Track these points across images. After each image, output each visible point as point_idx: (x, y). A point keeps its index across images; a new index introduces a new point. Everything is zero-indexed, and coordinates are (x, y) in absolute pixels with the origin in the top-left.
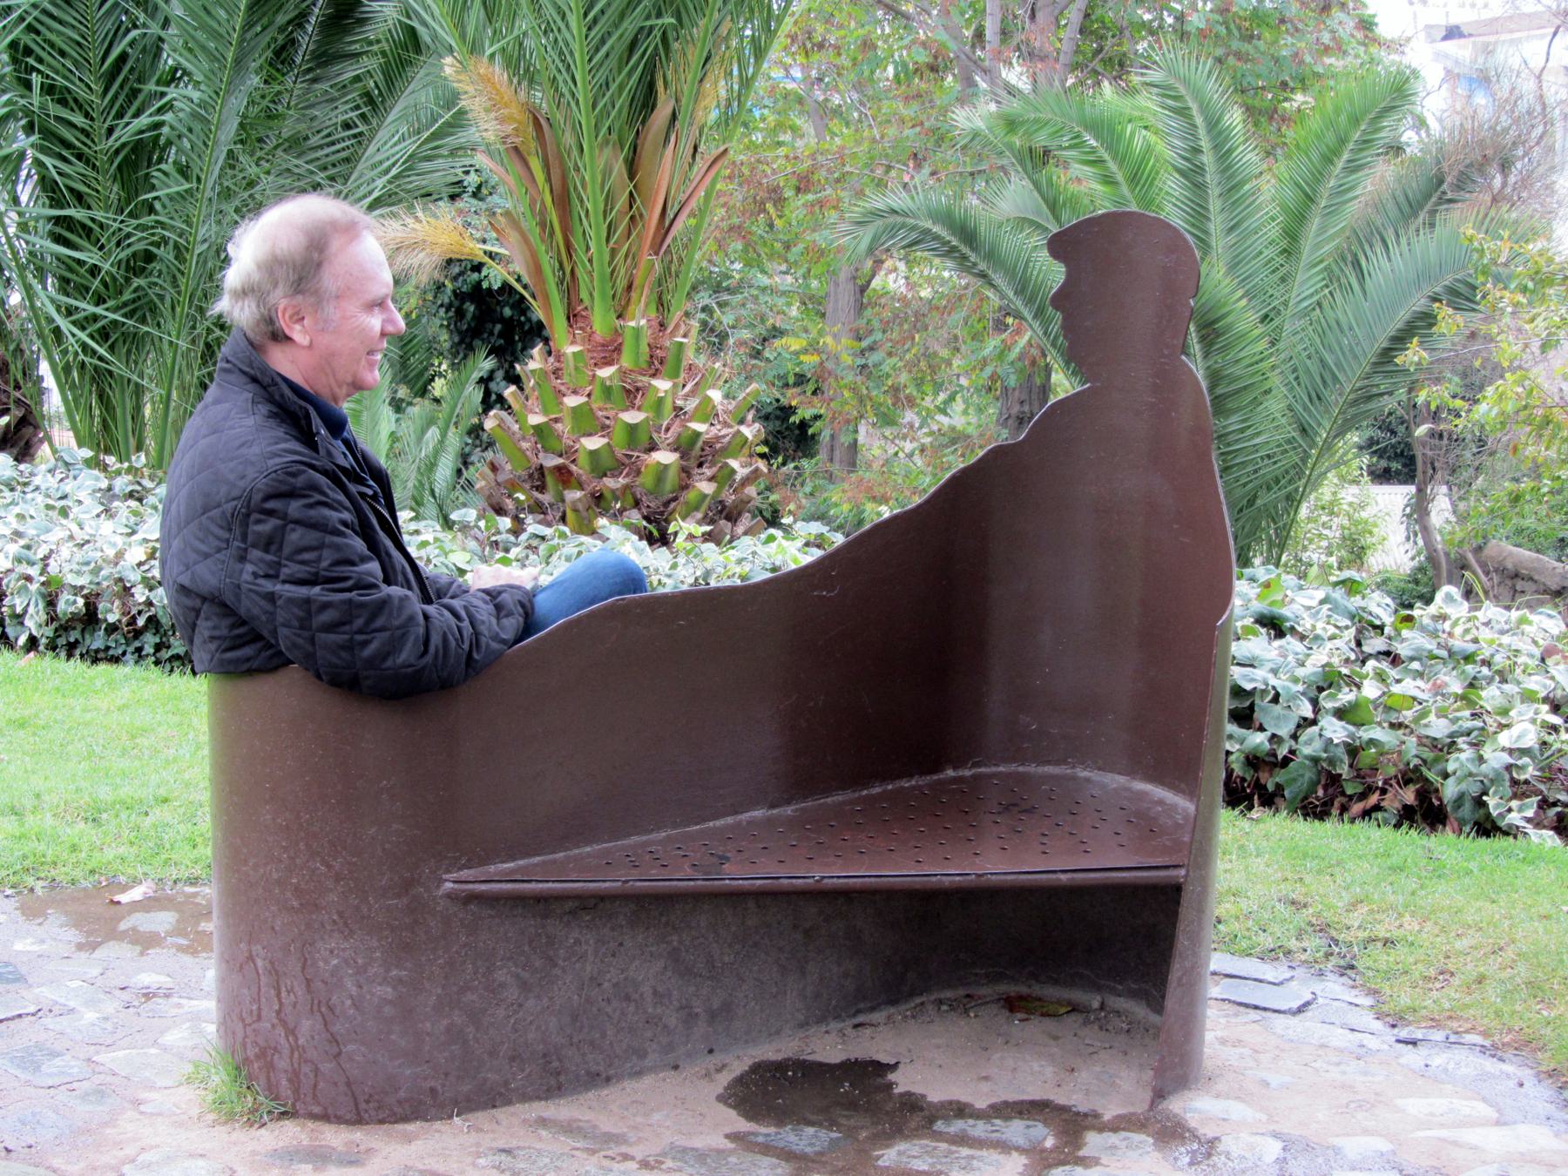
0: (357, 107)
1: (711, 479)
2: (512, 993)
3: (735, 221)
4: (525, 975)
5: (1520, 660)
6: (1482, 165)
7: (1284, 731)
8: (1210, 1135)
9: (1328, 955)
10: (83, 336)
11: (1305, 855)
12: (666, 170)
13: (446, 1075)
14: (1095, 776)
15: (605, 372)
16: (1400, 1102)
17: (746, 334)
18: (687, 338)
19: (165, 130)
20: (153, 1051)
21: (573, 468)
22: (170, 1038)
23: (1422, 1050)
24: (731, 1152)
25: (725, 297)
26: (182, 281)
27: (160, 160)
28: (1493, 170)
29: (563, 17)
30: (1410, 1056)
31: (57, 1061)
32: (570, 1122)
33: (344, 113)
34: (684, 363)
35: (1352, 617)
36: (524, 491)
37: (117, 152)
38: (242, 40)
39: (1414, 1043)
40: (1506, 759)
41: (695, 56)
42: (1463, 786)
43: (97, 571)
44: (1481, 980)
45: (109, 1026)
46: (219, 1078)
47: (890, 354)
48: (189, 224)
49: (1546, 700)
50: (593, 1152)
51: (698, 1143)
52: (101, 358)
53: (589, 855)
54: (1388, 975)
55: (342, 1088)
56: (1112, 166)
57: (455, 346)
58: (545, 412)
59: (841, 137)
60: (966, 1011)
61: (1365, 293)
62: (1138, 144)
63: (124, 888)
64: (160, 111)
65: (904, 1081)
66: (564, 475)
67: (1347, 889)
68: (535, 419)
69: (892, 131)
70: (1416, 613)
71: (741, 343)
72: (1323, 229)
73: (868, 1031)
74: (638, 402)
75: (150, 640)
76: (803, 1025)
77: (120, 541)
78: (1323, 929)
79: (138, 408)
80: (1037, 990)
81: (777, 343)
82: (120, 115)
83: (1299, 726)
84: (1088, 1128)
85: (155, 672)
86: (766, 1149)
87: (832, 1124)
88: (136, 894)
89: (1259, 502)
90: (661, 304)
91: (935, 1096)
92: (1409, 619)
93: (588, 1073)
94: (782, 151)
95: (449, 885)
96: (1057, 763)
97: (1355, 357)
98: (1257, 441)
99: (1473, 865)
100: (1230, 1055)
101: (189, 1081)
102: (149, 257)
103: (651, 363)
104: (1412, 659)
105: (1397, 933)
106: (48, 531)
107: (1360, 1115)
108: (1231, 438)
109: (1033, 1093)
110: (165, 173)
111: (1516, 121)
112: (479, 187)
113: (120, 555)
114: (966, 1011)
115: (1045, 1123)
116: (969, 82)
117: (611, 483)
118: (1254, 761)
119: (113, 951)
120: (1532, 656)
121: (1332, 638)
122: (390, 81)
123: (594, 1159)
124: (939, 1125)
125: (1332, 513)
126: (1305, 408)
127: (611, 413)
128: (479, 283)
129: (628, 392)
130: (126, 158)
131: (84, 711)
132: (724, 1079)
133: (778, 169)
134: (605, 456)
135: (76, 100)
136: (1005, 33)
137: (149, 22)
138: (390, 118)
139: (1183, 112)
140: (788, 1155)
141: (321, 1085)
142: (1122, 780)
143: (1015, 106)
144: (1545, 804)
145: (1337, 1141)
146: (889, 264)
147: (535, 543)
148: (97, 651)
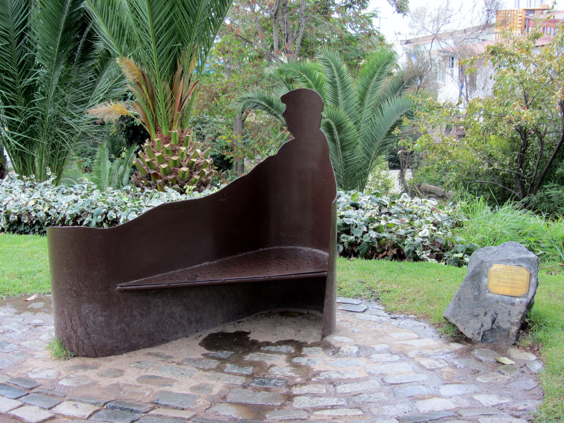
0: (93, 74)
1: (198, 175)
2: (139, 318)
3: (206, 103)
4: (142, 312)
5: (425, 213)
6: (414, 78)
7: (359, 235)
8: (338, 346)
9: (372, 296)
10: (16, 142)
11: (365, 269)
12: (181, 87)
13: (121, 342)
14: (302, 248)
15: (167, 146)
16: (391, 335)
17: (210, 135)
18: (191, 135)
19: (37, 82)
20: (37, 341)
21: (159, 173)
22: (42, 337)
23: (398, 320)
24: (203, 359)
25: (204, 125)
26: (44, 125)
27: (37, 91)
28: (418, 78)
29: (150, 45)
30: (395, 322)
31: (10, 345)
32: (157, 353)
33: (89, 75)
34: (189, 142)
35: (378, 203)
36: (144, 180)
37: (23, 89)
38: (58, 55)
39: (396, 318)
40: (421, 240)
41: (188, 55)
42: (409, 248)
43: (20, 208)
44: (414, 300)
45: (25, 335)
46: (56, 346)
47: (252, 139)
48: (46, 109)
49: (432, 223)
50: (163, 361)
51: (194, 357)
52: (22, 149)
53: (158, 277)
54: (389, 300)
55: (91, 347)
56: (310, 82)
57: (127, 142)
58: (150, 158)
59: (235, 78)
60: (269, 317)
61: (382, 114)
62: (317, 75)
63: (29, 296)
64: (35, 76)
65: (252, 337)
66: (156, 176)
67: (377, 277)
68: (147, 160)
69: (249, 75)
70: (396, 201)
71: (210, 138)
72: (371, 97)
73: (242, 324)
74: (176, 154)
75: (37, 227)
76: (223, 323)
77: (27, 199)
78: (370, 289)
79: (33, 164)
80: (289, 310)
81: (219, 137)
82: (24, 78)
83: (363, 234)
84: (303, 347)
85: (38, 236)
86: (213, 358)
87: (231, 350)
88: (33, 298)
89: (357, 175)
90: (182, 126)
91: (260, 340)
92: (394, 203)
93: (162, 339)
94: (218, 83)
95: (118, 287)
96: (291, 245)
97: (381, 133)
98: (355, 158)
99: (412, 269)
100: (344, 324)
101: (48, 348)
102: (34, 119)
103: (179, 143)
104: (395, 214)
105: (391, 289)
106: (6, 197)
107: (380, 339)
108: (347, 157)
109: (288, 338)
110: (38, 94)
111: (423, 65)
112: (132, 97)
113: (27, 203)
114: (269, 317)
115: (292, 346)
116: (270, 60)
117: (169, 177)
118: (351, 244)
119: (26, 314)
120: (428, 211)
121: (372, 209)
122: (102, 65)
123: (164, 363)
124: (262, 348)
125: (379, 178)
126: (368, 148)
127: (169, 157)
128: (133, 124)
129: (173, 151)
130: (26, 91)
131: (18, 248)
132: (201, 339)
133: (217, 88)
134: (168, 170)
135: (10, 74)
136: (279, 47)
137: (31, 51)
138: (103, 77)
139: (330, 66)
140: (219, 359)
141: (85, 347)
142: (310, 249)
143: (282, 67)
144: (432, 252)
145: (373, 346)
146: (250, 114)
147: (147, 194)
148: (22, 231)
